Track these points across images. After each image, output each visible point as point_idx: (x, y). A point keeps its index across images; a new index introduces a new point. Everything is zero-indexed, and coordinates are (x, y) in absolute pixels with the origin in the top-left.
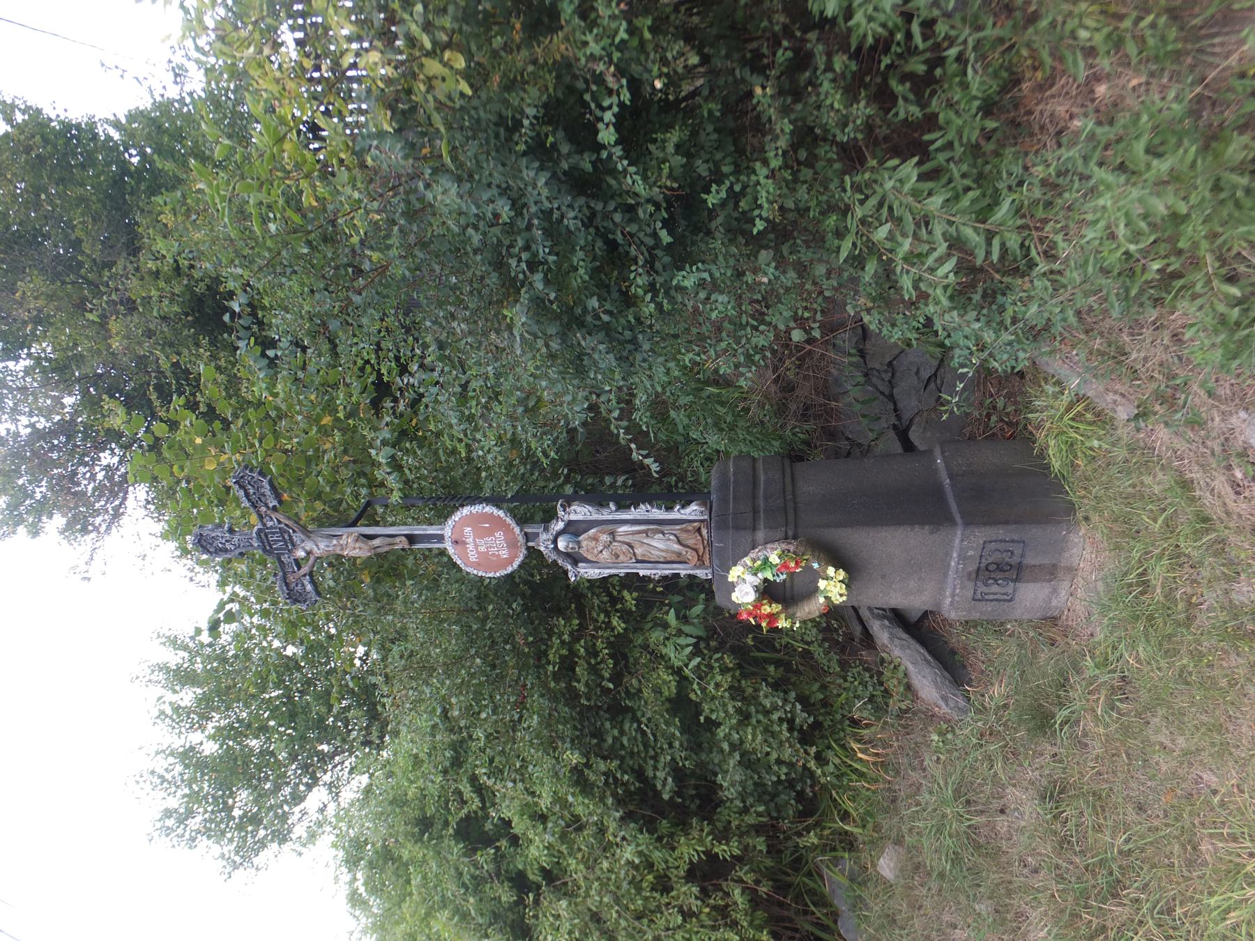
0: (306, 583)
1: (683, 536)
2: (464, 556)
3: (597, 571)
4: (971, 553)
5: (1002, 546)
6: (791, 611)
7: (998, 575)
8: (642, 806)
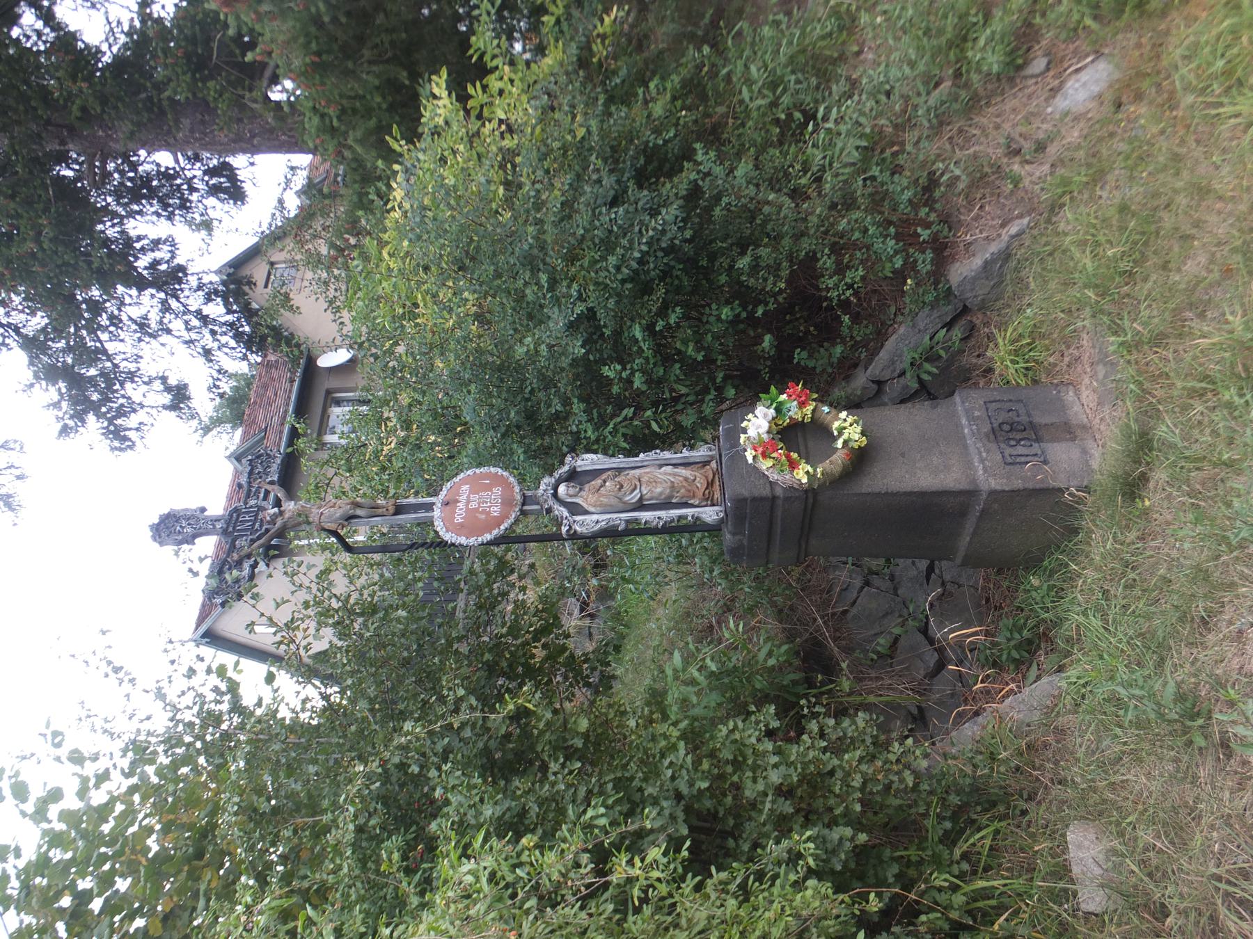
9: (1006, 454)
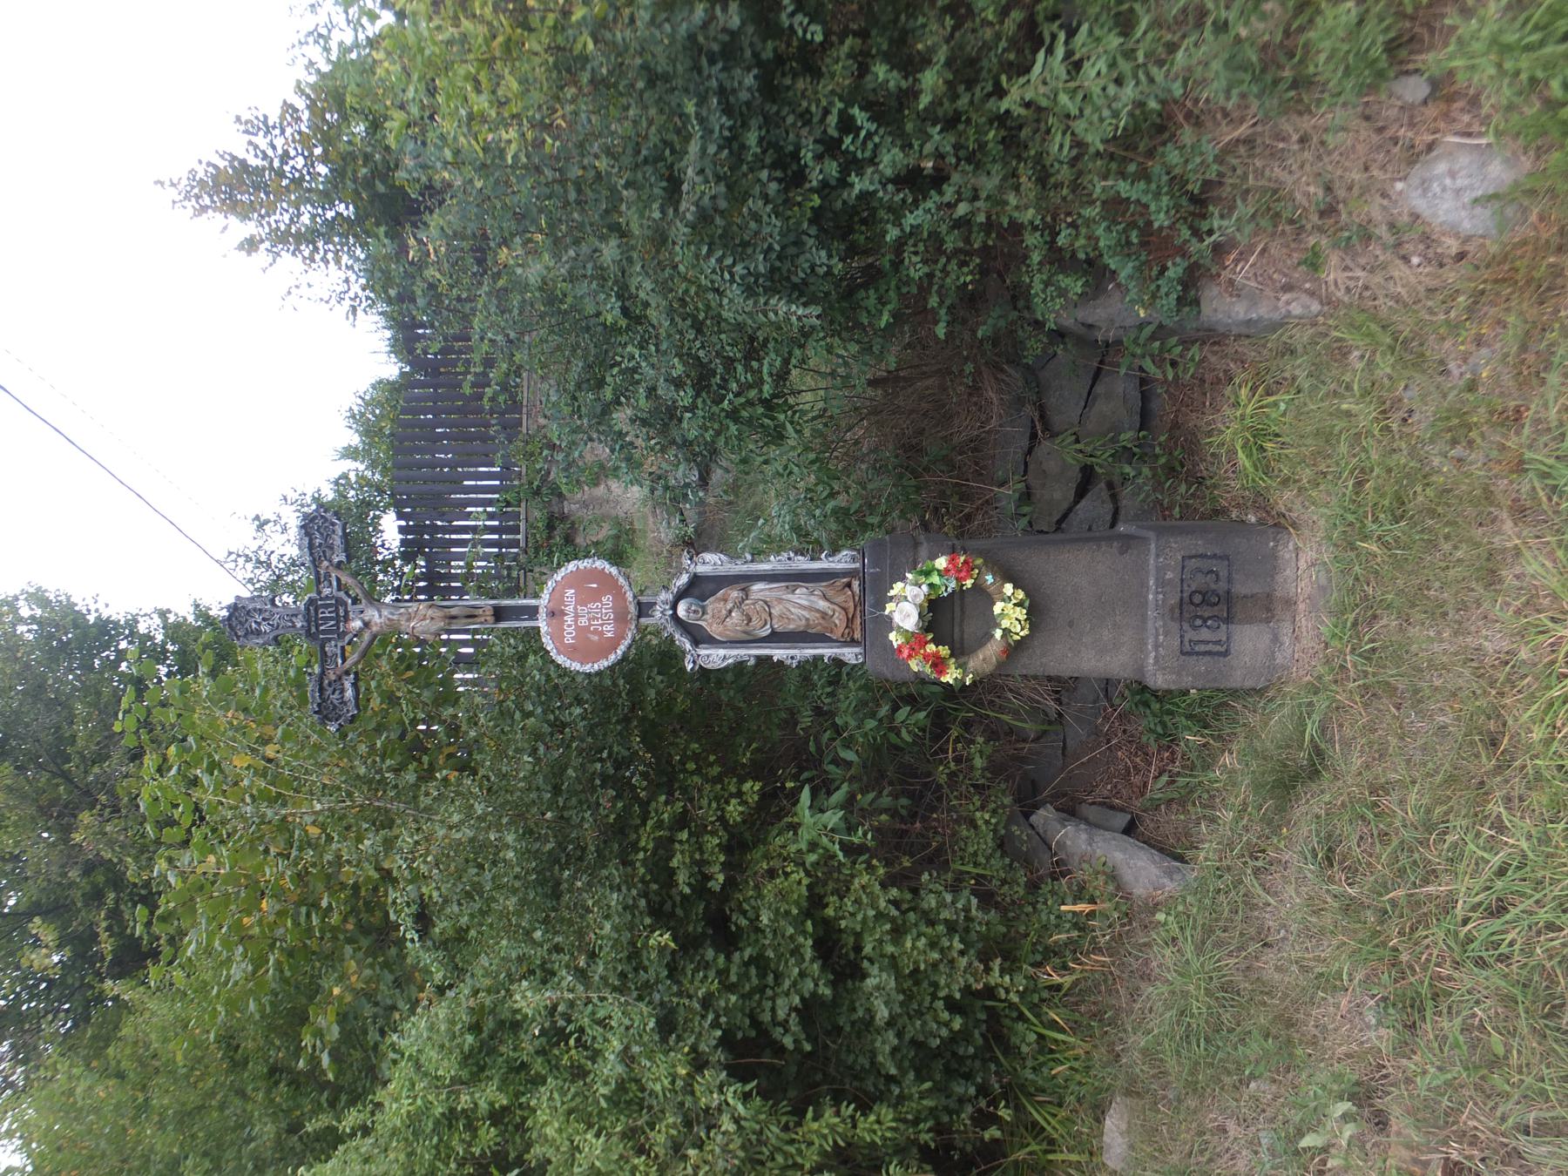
0: (347, 685)
1: (830, 593)
2: (557, 636)
3: (722, 652)
4: (1169, 575)
5: (1205, 564)
6: (962, 660)
7: (1207, 612)
8: (748, 1055)
9: (1186, 639)
